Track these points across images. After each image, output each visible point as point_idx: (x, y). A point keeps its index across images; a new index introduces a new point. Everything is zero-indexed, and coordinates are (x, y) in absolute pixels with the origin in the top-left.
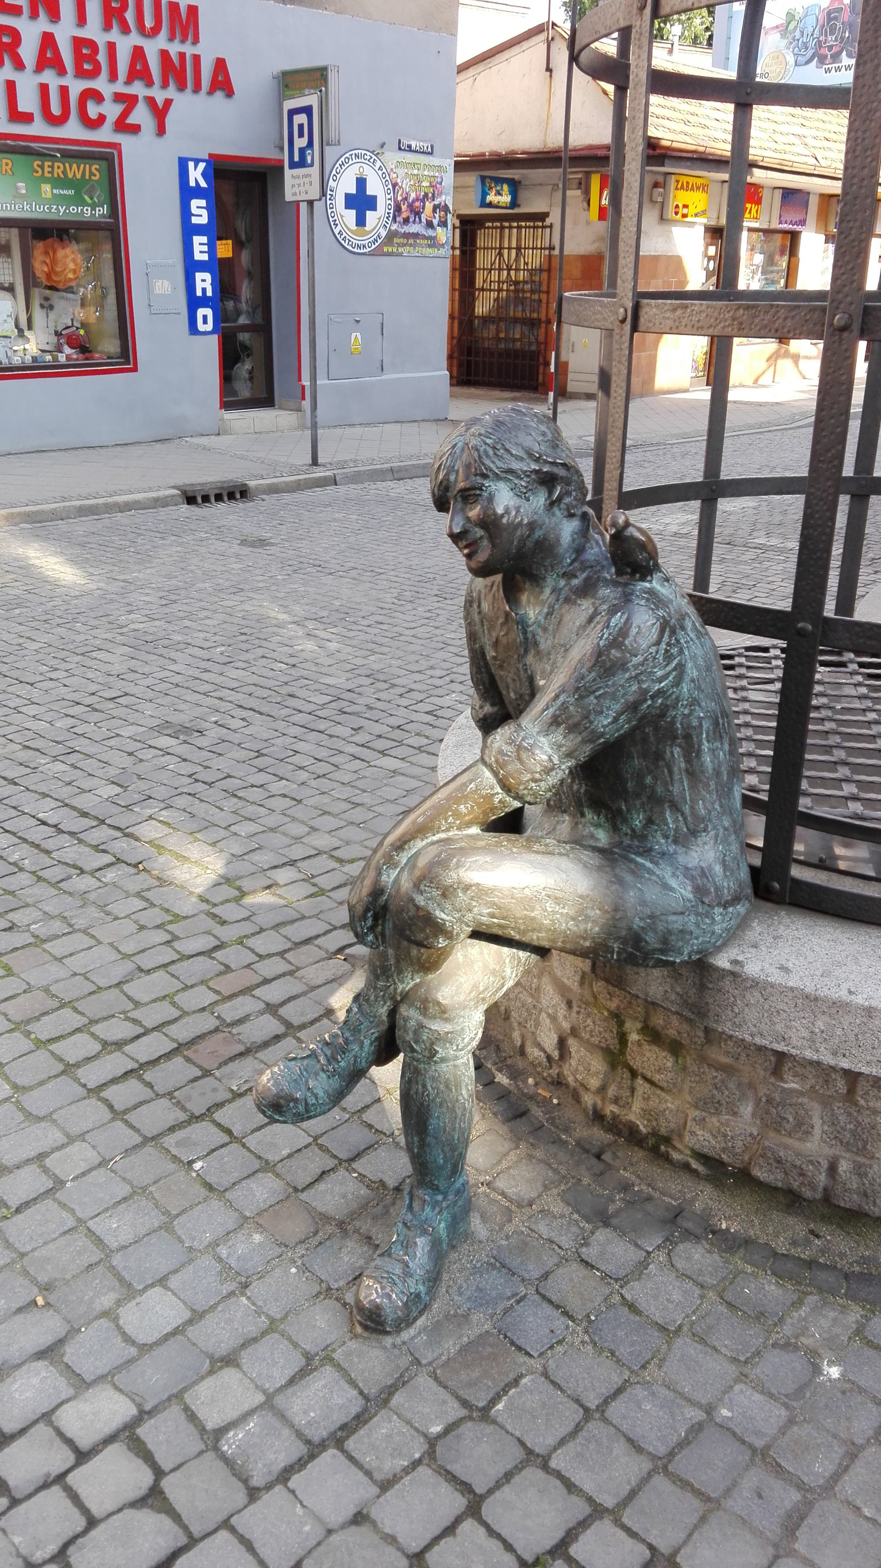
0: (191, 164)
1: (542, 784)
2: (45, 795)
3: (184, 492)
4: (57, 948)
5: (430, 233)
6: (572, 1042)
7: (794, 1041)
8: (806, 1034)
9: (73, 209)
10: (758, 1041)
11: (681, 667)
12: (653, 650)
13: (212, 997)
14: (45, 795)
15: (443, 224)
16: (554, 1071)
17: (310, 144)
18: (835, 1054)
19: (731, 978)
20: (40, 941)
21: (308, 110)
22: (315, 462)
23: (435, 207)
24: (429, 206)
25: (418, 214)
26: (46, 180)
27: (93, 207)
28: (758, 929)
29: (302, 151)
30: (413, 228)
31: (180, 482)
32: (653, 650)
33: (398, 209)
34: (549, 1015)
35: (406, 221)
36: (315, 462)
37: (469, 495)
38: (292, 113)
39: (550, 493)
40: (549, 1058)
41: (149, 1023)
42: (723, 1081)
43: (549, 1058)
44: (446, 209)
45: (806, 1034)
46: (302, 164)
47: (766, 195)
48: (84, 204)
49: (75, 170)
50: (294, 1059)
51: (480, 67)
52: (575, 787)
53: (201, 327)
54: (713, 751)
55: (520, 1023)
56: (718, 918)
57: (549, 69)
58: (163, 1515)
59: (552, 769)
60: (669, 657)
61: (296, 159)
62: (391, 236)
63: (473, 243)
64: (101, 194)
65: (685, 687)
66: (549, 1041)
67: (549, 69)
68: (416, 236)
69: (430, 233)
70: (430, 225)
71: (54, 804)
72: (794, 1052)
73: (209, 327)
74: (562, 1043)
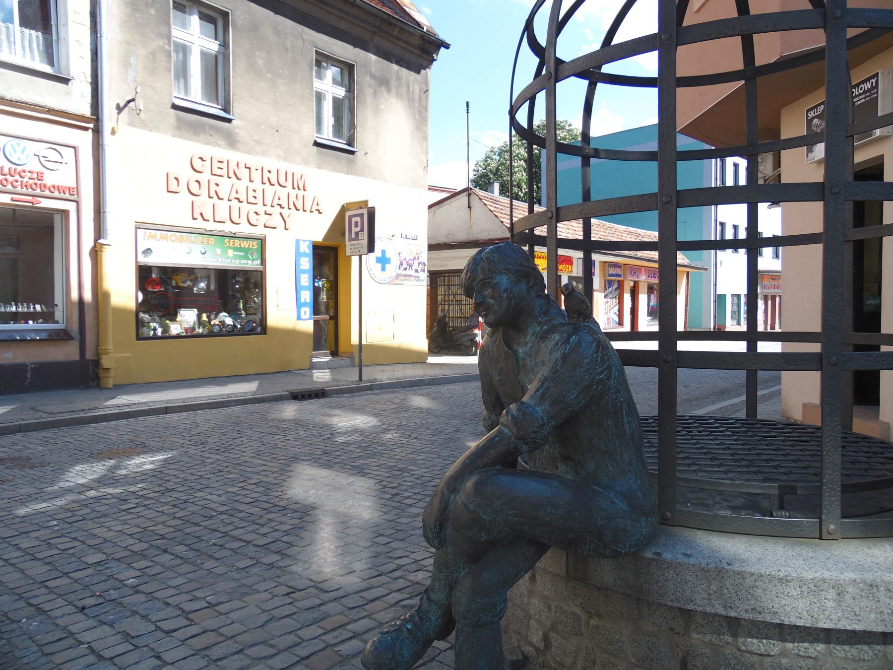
0: (301, 243)
1: (539, 434)
2: (215, 530)
3: (292, 393)
4: (222, 608)
5: (416, 274)
6: (552, 635)
7: (698, 602)
8: (705, 596)
9: (243, 261)
10: (675, 604)
11: (609, 367)
12: (595, 355)
13: (320, 631)
14: (215, 530)
15: (423, 271)
16: (540, 660)
17: (362, 230)
18: (725, 607)
19: (655, 563)
20: (211, 605)
21: (361, 215)
22: (361, 379)
23: (419, 263)
24: (416, 262)
25: (411, 266)
26: (230, 248)
27: (253, 260)
28: (664, 538)
29: (357, 233)
30: (407, 272)
31: (290, 388)
32: (595, 355)
33: (401, 264)
34: (536, 620)
35: (405, 269)
36: (361, 379)
37: (485, 284)
38: (350, 217)
39: (528, 283)
40: (537, 650)
41: (282, 646)
42: (653, 643)
43: (537, 650)
44: (424, 264)
45: (705, 596)
46: (357, 238)
47: (575, 261)
48: (249, 259)
49: (245, 244)
50: (387, 632)
51: (437, 207)
52: (551, 451)
53: (303, 316)
54: (629, 422)
55: (515, 632)
56: (644, 524)
57: (469, 207)
58: (595, 316)
59: (544, 425)
60: (603, 361)
61: (353, 236)
62: (398, 276)
63: (436, 283)
64: (257, 255)
65: (612, 382)
66: (536, 638)
67: (469, 207)
68: (410, 276)
69: (416, 274)
70: (417, 271)
71: (220, 535)
72: (699, 609)
73: (308, 316)
74: (546, 639)
